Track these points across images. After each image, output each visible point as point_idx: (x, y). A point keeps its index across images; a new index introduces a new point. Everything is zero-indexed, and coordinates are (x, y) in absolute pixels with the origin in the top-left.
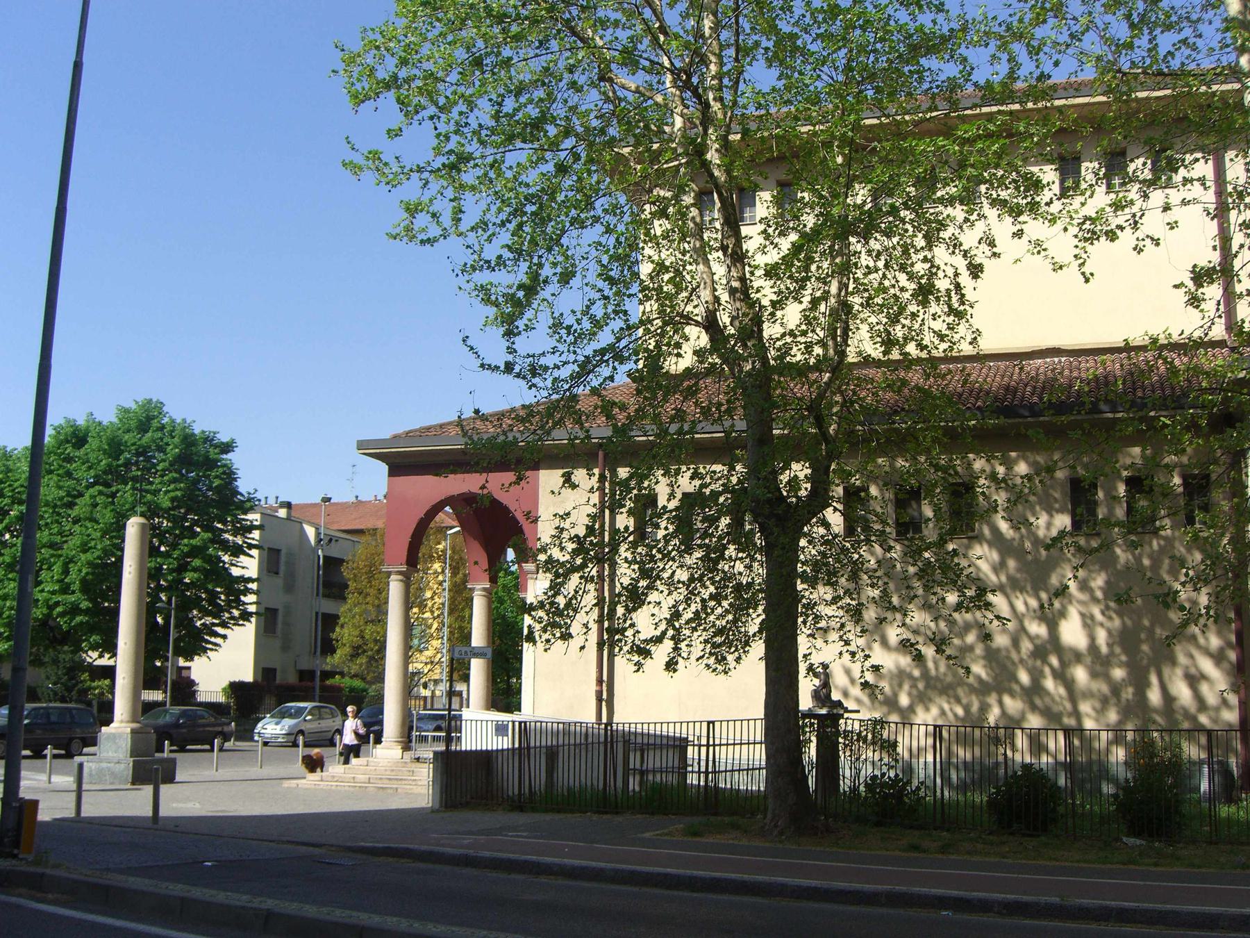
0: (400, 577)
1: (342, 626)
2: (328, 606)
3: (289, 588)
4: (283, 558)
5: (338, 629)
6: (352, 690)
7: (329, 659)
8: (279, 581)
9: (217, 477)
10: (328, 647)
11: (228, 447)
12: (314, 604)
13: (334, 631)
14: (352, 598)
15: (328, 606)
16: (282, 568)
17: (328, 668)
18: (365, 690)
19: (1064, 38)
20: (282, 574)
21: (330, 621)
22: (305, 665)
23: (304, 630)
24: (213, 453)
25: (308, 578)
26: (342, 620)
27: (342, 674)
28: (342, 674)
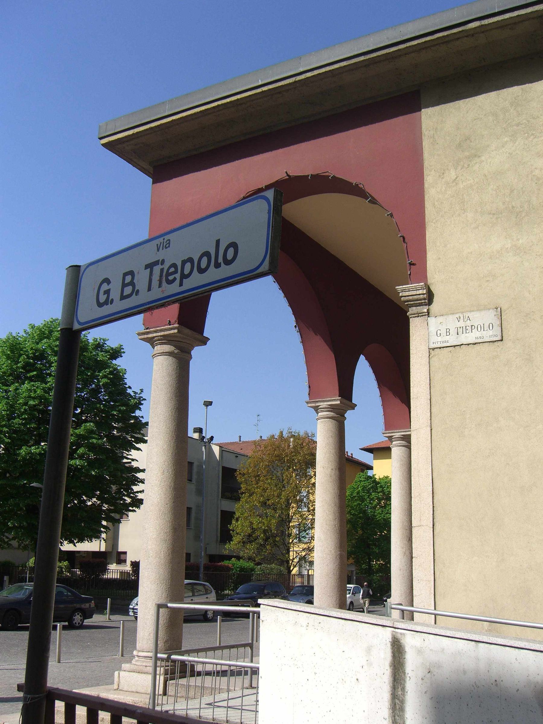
0: (167, 348)
1: (237, 520)
2: (226, 505)
3: (199, 492)
4: (195, 469)
5: (234, 522)
6: (242, 569)
7: (227, 546)
8: (192, 487)
9: (105, 377)
10: (226, 536)
11: (116, 353)
12: (214, 503)
13: (231, 523)
14: (244, 498)
15: (226, 505)
16: (195, 477)
17: (226, 553)
18: (252, 570)
19: (526, 421)
20: (194, 481)
21: (227, 517)
22: (213, 550)
23: (212, 522)
24: (101, 356)
25: (214, 483)
26: (237, 515)
27: (238, 558)
28: (238, 558)
